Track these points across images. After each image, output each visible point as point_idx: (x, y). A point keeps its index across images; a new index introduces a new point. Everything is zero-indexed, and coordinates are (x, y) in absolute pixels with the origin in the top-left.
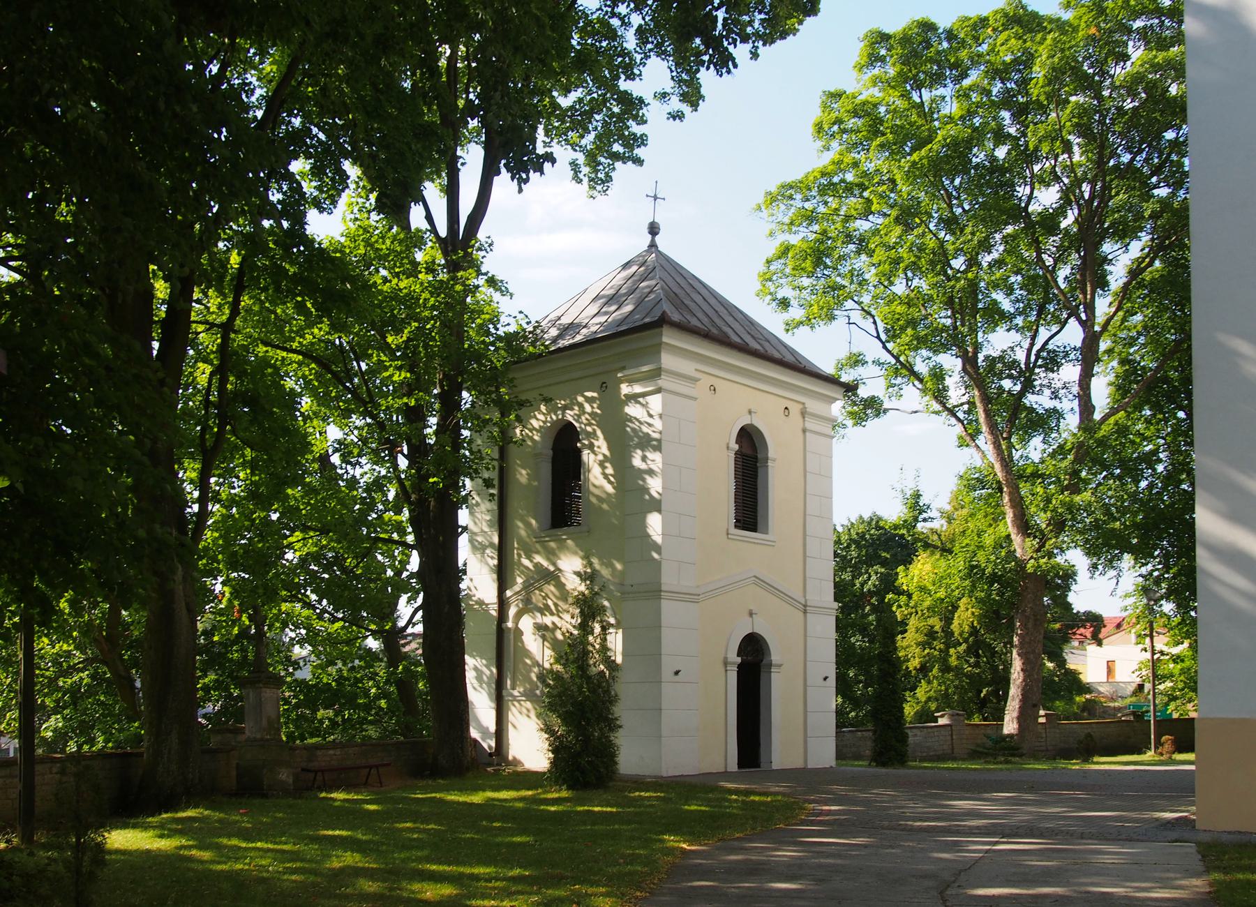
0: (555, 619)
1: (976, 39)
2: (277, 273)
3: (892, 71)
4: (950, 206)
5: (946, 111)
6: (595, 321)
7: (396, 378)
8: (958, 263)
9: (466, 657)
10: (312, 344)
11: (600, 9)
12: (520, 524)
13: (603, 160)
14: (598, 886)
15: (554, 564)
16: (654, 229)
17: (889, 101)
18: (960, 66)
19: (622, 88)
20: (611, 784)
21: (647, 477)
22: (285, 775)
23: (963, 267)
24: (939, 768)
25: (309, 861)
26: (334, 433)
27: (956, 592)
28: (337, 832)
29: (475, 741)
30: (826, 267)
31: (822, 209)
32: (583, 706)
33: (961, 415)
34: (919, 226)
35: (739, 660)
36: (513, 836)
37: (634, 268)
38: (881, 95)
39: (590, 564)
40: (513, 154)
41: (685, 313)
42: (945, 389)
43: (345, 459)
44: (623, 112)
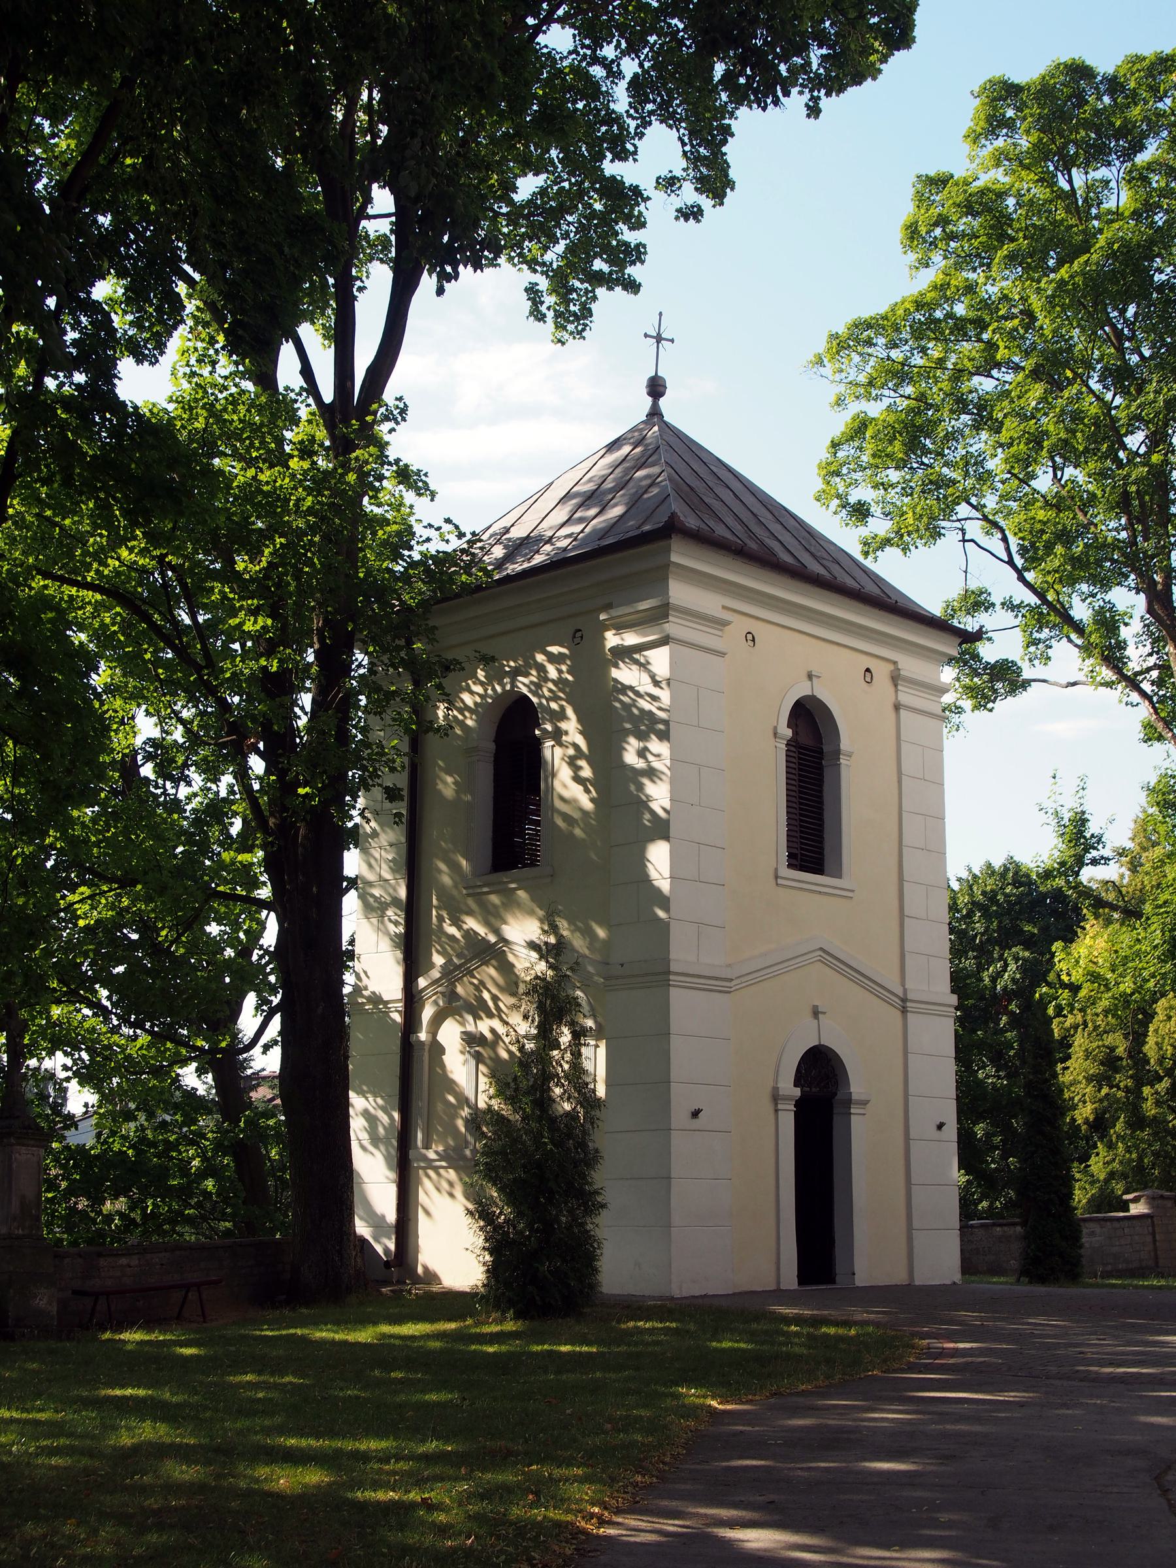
0: (496, 1024)
1: (1153, 89)
2: (66, 452)
3: (1024, 143)
4: (1121, 350)
5: (1110, 204)
6: (560, 529)
7: (248, 626)
8: (1135, 441)
9: (352, 1094)
10: (118, 573)
11: (575, 52)
12: (443, 866)
13: (577, 284)
14: (569, 1465)
15: (497, 931)
16: (656, 388)
17: (1019, 188)
18: (1129, 132)
19: (607, 173)
20: (587, 1310)
21: (645, 781)
22: (44, 1301)
23: (1142, 450)
24: (1136, 1287)
25: (81, 1437)
26: (146, 727)
27: (1151, 984)
28: (129, 1392)
29: (363, 1241)
30: (926, 452)
31: (918, 360)
32: (540, 1173)
33: (1146, 687)
34: (1071, 383)
35: (797, 1092)
36: (424, 1392)
37: (626, 449)
38: (1007, 180)
39: (554, 929)
40: (438, 241)
41: (705, 517)
42: (1122, 646)
43: (163, 771)
44: (609, 210)
